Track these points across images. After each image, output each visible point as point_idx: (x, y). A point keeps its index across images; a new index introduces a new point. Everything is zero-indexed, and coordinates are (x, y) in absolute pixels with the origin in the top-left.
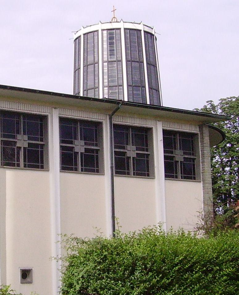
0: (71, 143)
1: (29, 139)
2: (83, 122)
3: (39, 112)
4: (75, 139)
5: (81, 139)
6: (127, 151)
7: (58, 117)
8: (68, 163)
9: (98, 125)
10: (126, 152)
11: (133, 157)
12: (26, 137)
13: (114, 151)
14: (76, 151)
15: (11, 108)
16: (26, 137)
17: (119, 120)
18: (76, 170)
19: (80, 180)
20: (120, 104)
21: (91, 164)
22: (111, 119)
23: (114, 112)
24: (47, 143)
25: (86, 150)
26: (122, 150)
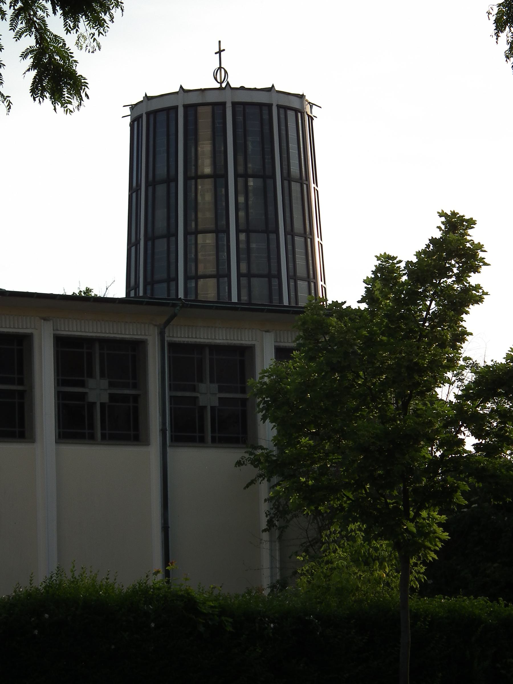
0: (82, 384)
1: (221, 390)
2: (105, 342)
3: (81, 331)
4: (201, 381)
5: (212, 381)
6: (198, 395)
7: (273, 348)
8: (74, 424)
9: (137, 347)
10: (198, 397)
11: (211, 407)
12: (215, 387)
13: (171, 397)
14: (201, 404)
15: (143, 334)
16: (215, 387)
17: (182, 335)
18: (202, 440)
19: (99, 460)
20: (178, 308)
21: (123, 426)
22: (162, 334)
23: (167, 323)
24: (31, 387)
25: (112, 397)
26: (188, 394)
